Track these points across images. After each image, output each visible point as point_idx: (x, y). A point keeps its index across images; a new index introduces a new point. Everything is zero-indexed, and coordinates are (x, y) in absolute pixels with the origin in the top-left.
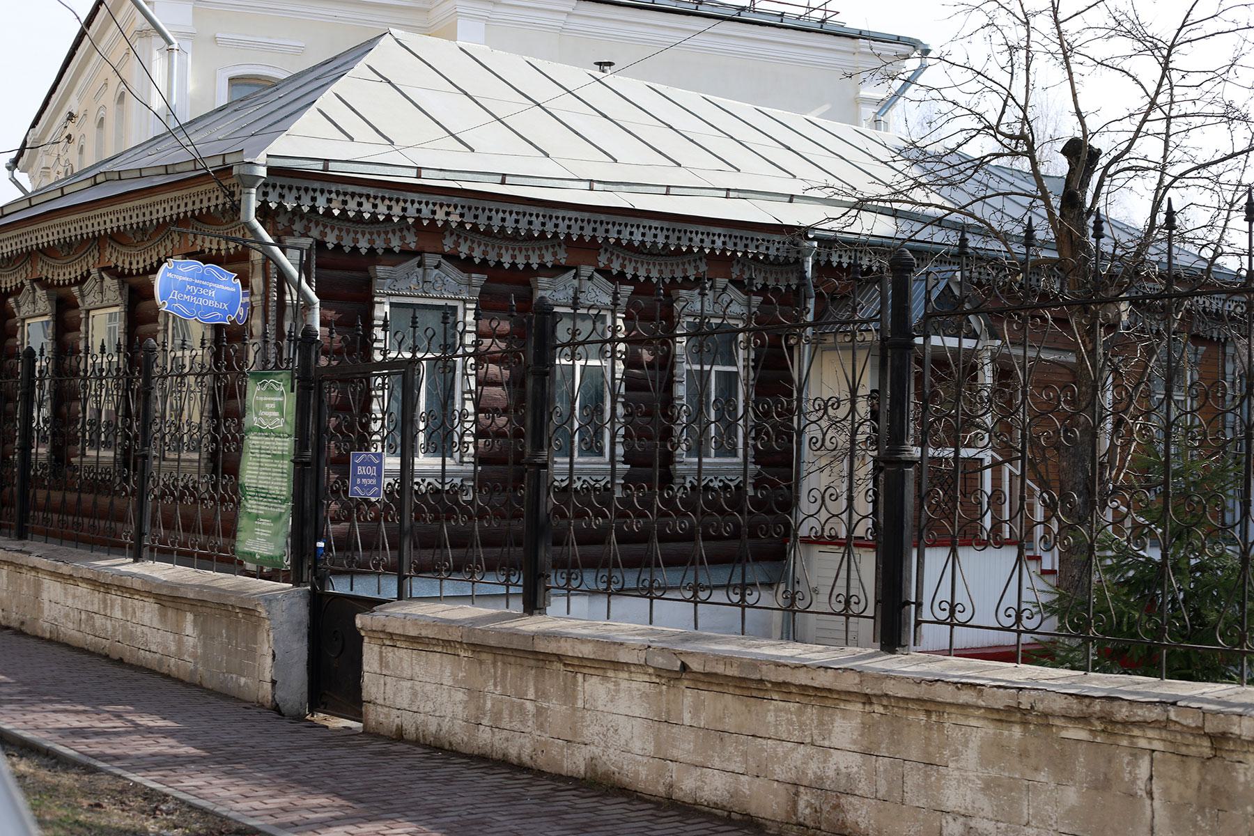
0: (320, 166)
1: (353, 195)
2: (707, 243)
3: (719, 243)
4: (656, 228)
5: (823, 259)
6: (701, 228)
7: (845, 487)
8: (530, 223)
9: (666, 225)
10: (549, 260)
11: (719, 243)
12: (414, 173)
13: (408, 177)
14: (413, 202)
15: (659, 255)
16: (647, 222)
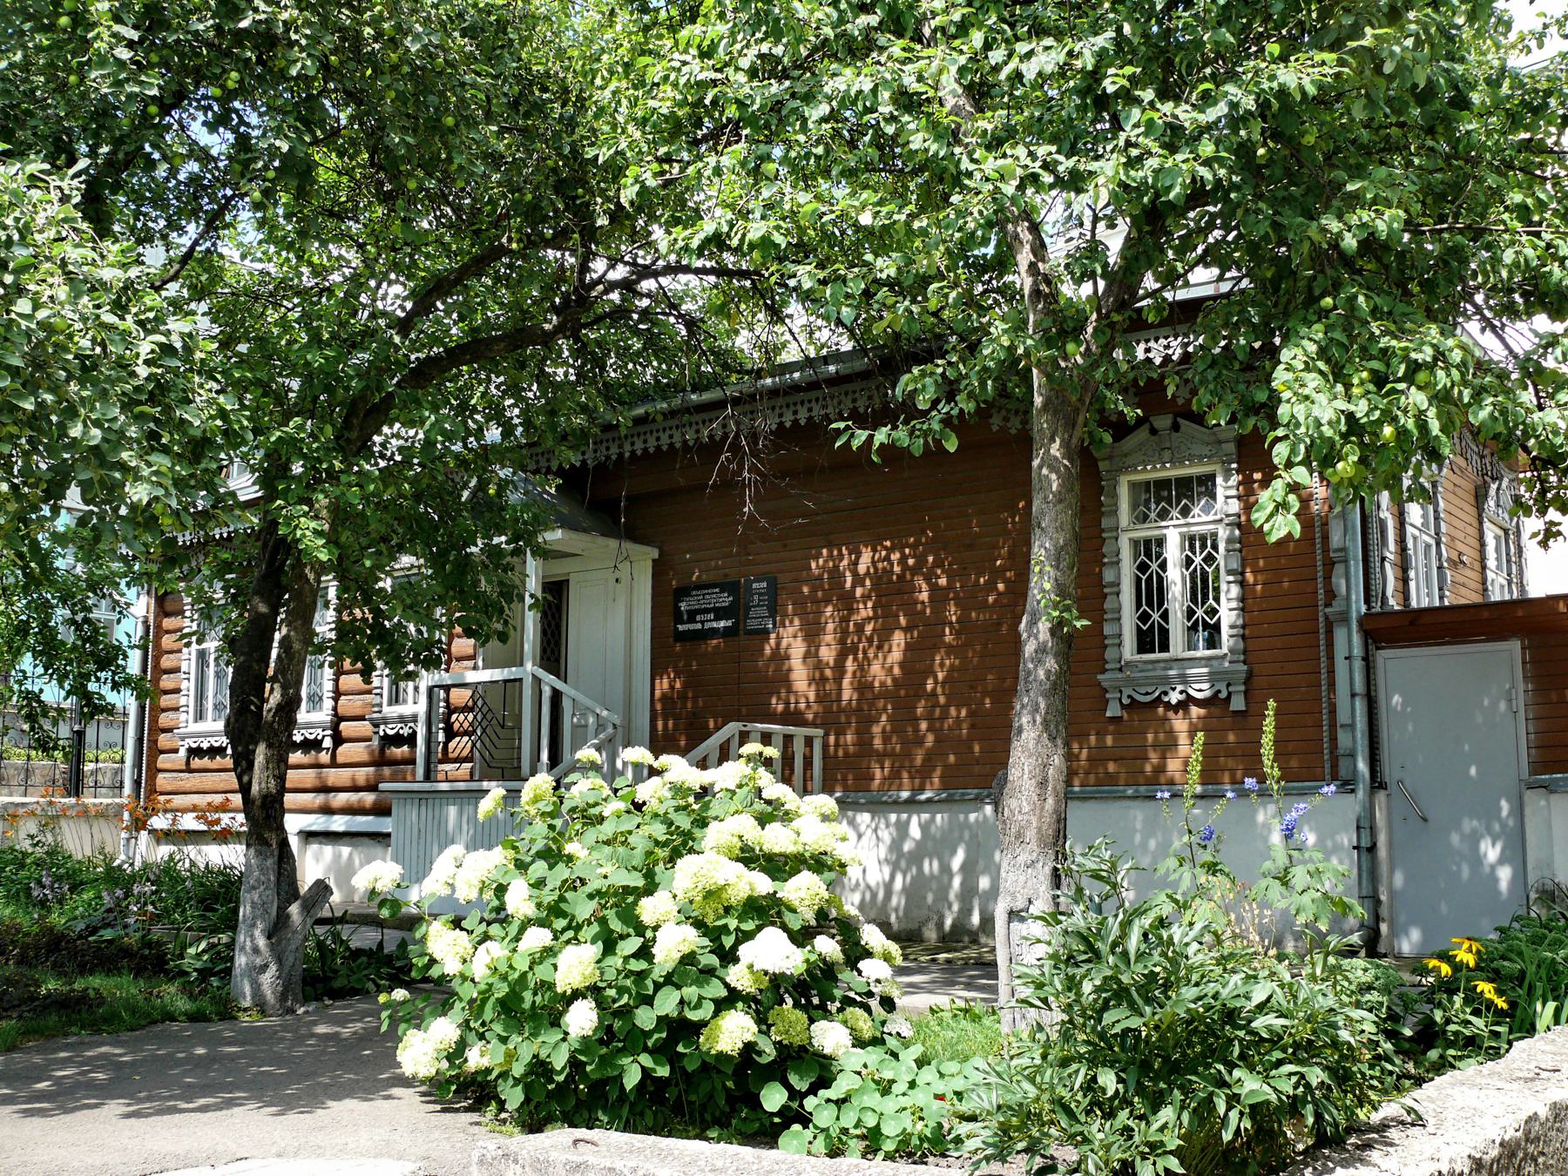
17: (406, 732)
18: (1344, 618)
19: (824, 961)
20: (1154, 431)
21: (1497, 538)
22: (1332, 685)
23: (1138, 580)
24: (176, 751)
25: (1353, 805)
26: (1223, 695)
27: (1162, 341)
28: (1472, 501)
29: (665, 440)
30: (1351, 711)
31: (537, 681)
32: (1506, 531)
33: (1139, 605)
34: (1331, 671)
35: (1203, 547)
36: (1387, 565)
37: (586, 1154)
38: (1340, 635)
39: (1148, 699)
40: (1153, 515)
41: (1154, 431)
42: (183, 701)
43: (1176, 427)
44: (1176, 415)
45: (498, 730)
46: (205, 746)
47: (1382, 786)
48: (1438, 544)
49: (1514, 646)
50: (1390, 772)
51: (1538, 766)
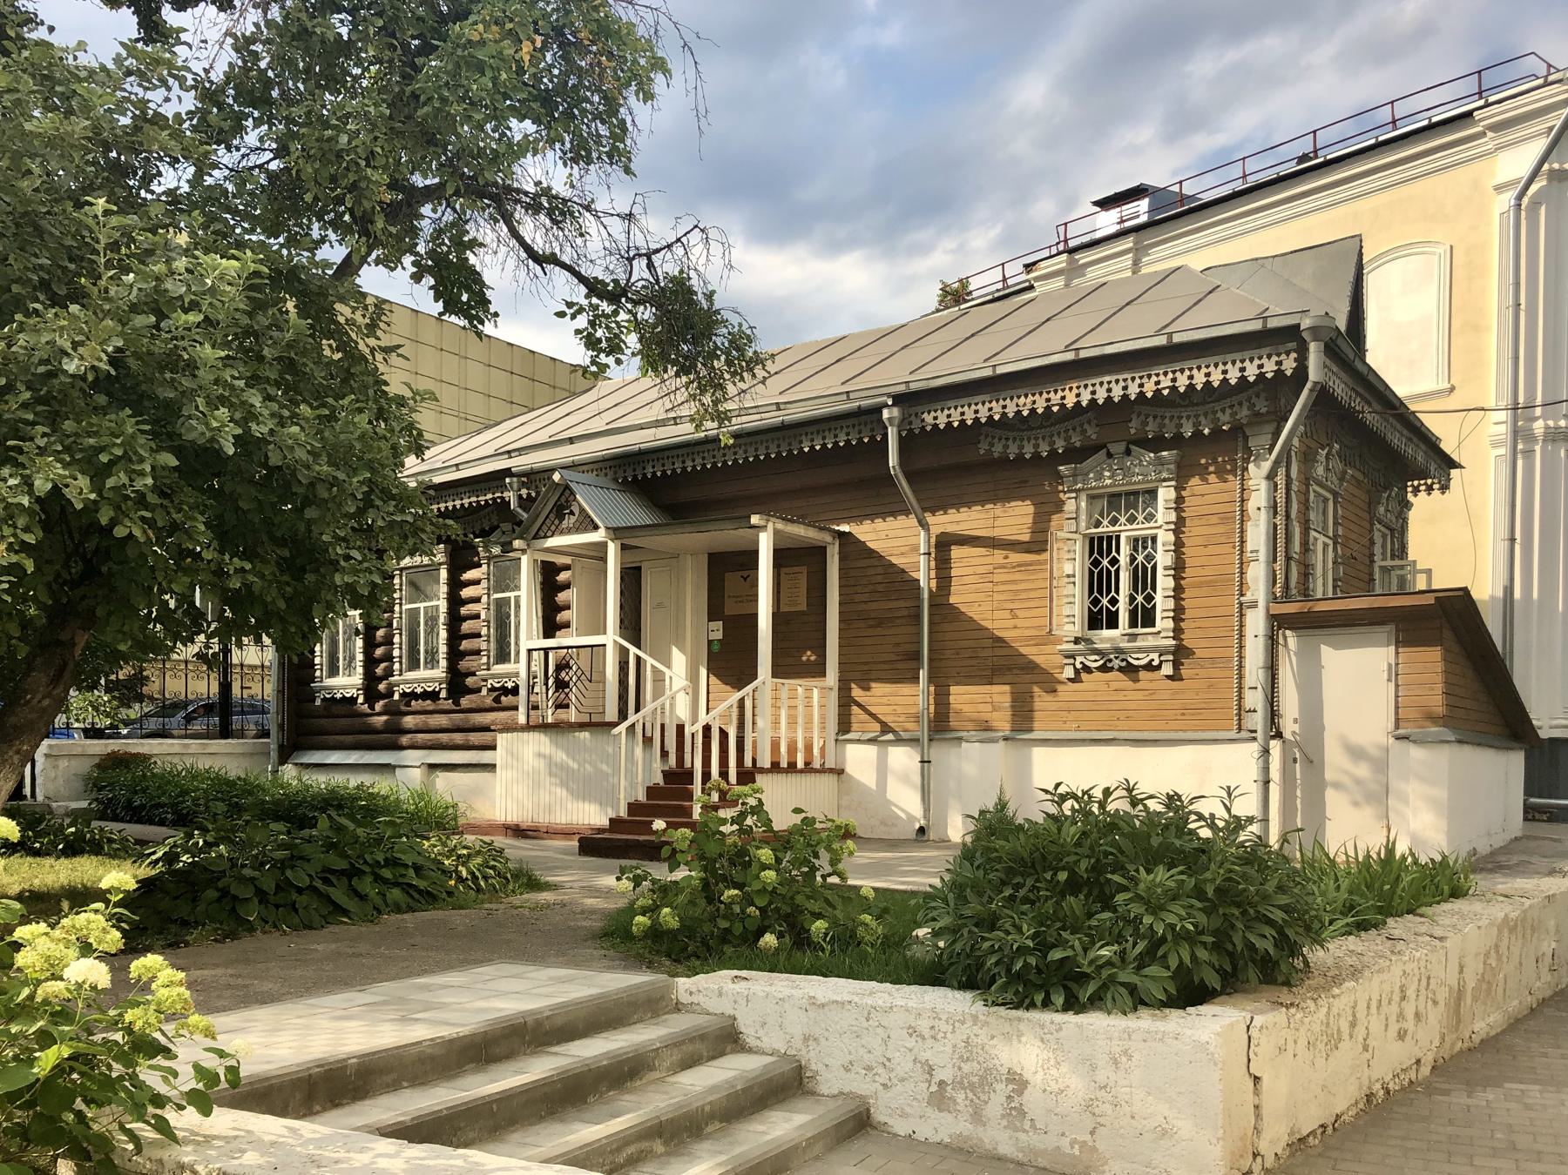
10: (1076, 441)
17: (510, 685)
20: (1110, 455)
21: (1384, 536)
23: (1091, 573)
24: (479, 690)
25: (1254, 748)
27: (1002, 402)
29: (689, 464)
31: (624, 652)
33: (1091, 592)
35: (1145, 548)
37: (741, 986)
41: (1110, 455)
42: (484, 646)
43: (1128, 452)
45: (587, 683)
46: (419, 690)
48: (1335, 544)
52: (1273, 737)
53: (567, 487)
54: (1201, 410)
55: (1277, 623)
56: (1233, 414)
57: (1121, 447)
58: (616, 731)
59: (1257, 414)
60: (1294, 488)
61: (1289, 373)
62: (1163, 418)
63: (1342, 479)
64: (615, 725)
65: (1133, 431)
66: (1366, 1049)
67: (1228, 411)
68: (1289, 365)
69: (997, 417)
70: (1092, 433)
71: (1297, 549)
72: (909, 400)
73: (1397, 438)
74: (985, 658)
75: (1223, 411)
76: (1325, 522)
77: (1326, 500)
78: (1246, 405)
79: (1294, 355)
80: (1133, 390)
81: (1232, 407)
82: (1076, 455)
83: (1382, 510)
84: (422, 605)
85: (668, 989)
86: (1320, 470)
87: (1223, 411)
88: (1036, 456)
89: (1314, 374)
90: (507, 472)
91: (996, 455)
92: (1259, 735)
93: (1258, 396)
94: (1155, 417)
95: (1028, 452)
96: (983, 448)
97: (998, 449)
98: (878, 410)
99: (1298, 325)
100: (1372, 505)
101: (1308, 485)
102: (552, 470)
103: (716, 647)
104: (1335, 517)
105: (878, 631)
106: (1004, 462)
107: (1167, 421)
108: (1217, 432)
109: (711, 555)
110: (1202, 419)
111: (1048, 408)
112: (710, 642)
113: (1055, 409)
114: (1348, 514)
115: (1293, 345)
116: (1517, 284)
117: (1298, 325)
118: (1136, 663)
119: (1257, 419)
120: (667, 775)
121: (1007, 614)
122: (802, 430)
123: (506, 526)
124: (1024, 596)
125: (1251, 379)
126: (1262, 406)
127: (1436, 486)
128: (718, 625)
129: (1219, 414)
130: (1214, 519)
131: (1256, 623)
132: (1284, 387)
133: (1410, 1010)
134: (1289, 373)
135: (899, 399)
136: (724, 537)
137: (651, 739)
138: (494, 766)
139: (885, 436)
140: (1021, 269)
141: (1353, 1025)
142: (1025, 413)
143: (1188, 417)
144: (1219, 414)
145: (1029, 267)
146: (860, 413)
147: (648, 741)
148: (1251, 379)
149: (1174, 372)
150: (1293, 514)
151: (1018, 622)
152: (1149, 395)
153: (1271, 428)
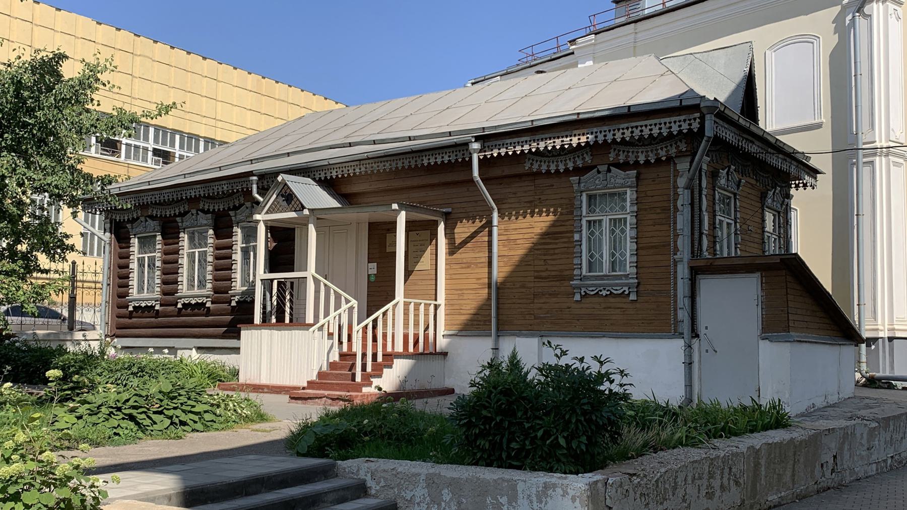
0: (626, 110)
1: (637, 127)
2: (220, 190)
3: (225, 188)
4: (680, 121)
5: (260, 184)
6: (217, 183)
7: (341, 402)
8: (641, 131)
9: (203, 185)
10: (580, 163)
11: (225, 188)
12: (530, 124)
13: (529, 125)
14: (675, 122)
15: (559, 155)
16: (195, 187)
18: (681, 260)
19: (324, 502)
20: (599, 172)
22: (675, 290)
25: (679, 343)
26: (627, 293)
28: (758, 200)
30: (683, 301)
32: (779, 213)
34: (676, 284)
36: (704, 237)
38: (680, 268)
39: (592, 293)
40: (597, 210)
43: (609, 171)
44: (610, 165)
47: (697, 336)
48: (735, 223)
49: (758, 275)
50: (702, 331)
51: (269, 224)
52: (693, 337)
53: (286, 184)
54: (649, 148)
55: (695, 272)
56: (667, 151)
57: (605, 168)
58: (312, 329)
59: (681, 151)
60: (704, 192)
61: (695, 130)
62: (628, 152)
63: (738, 186)
64: (311, 325)
65: (611, 159)
66: (684, 501)
67: (665, 149)
68: (695, 126)
69: (534, 150)
70: (588, 159)
71: (706, 228)
72: (487, 138)
73: (775, 161)
74: (530, 288)
75: (662, 149)
76: (730, 210)
77: (729, 198)
78: (674, 146)
79: (698, 120)
80: (610, 138)
81: (666, 147)
82: (580, 171)
83: (770, 201)
84: (197, 250)
85: (334, 466)
86: (723, 182)
87: (662, 149)
88: (557, 171)
89: (709, 132)
90: (251, 173)
91: (535, 170)
92: (685, 335)
93: (681, 141)
94: (624, 151)
95: (553, 168)
96: (527, 166)
97: (535, 167)
98: (466, 144)
99: (699, 105)
100: (763, 197)
101: (714, 190)
102: (277, 174)
103: (373, 279)
104: (735, 207)
105: (469, 271)
106: (538, 174)
107: (630, 154)
108: (658, 161)
109: (370, 224)
110: (650, 153)
111: (562, 146)
112: (369, 276)
113: (566, 146)
114: (744, 205)
115: (697, 115)
116: (394, 320)
117: (699, 105)
118: (615, 292)
119: (680, 155)
120: (342, 356)
121: (542, 263)
122: (423, 154)
123: (248, 204)
124: (552, 252)
125: (675, 133)
126: (683, 147)
127: (801, 185)
128: (374, 265)
129: (660, 151)
130: (658, 211)
131: (683, 271)
132: (694, 137)
133: (716, 483)
134: (695, 130)
135: (477, 139)
136: (379, 214)
137: (332, 334)
138: (239, 348)
139: (471, 158)
140: (331, 331)
141: (675, 488)
142: (550, 148)
143: (642, 152)
144: (660, 151)
145: (573, 42)
146: (456, 145)
147: (330, 335)
148: (675, 133)
149: (632, 128)
150: (704, 208)
151: (550, 268)
152: (619, 140)
153: (689, 159)
